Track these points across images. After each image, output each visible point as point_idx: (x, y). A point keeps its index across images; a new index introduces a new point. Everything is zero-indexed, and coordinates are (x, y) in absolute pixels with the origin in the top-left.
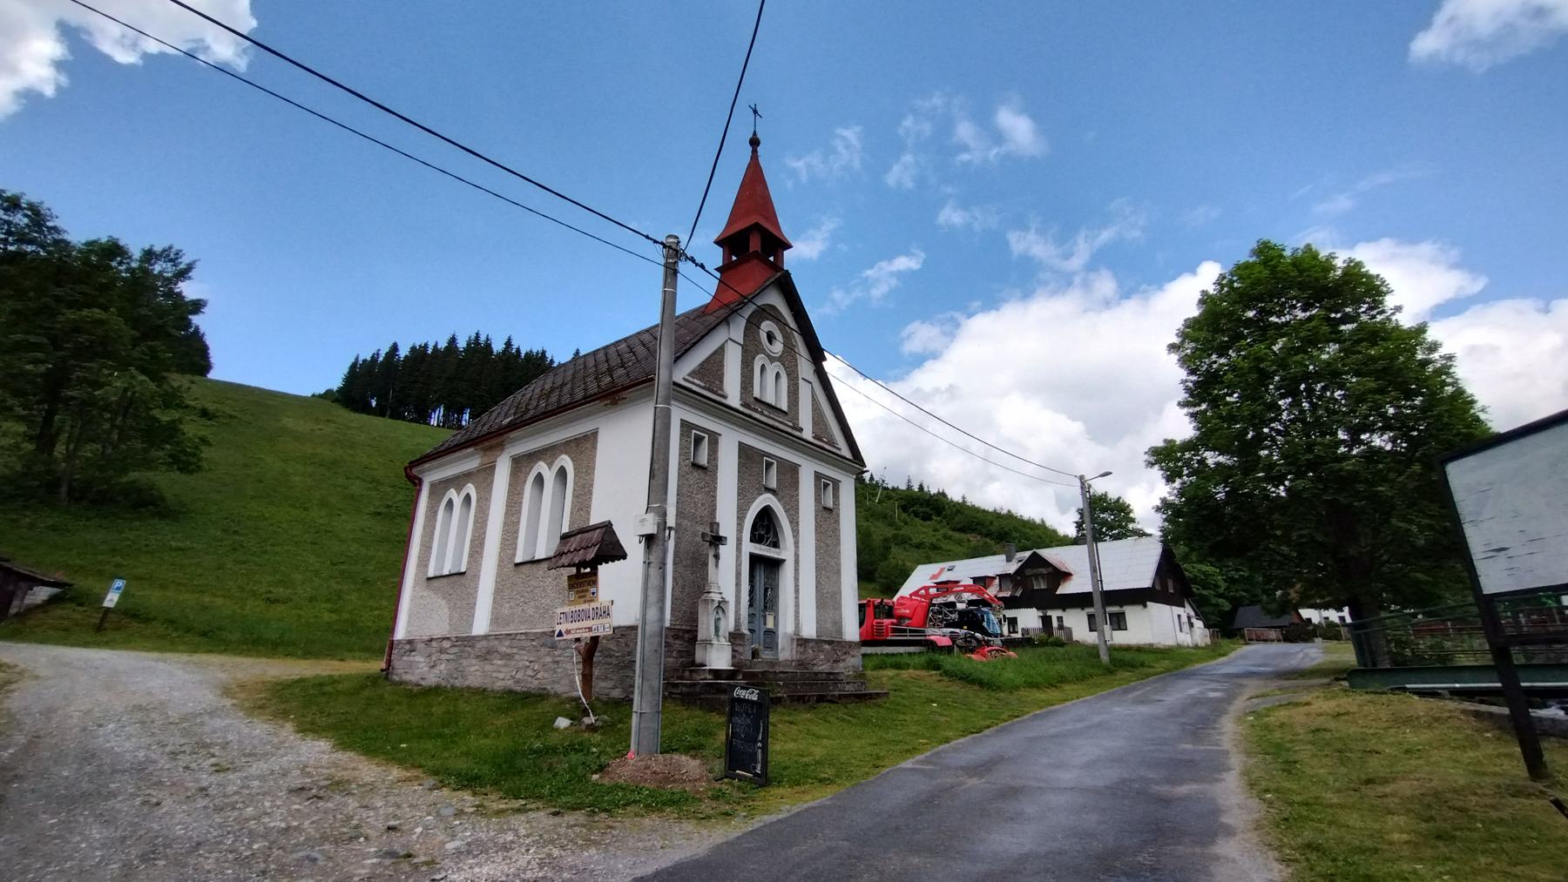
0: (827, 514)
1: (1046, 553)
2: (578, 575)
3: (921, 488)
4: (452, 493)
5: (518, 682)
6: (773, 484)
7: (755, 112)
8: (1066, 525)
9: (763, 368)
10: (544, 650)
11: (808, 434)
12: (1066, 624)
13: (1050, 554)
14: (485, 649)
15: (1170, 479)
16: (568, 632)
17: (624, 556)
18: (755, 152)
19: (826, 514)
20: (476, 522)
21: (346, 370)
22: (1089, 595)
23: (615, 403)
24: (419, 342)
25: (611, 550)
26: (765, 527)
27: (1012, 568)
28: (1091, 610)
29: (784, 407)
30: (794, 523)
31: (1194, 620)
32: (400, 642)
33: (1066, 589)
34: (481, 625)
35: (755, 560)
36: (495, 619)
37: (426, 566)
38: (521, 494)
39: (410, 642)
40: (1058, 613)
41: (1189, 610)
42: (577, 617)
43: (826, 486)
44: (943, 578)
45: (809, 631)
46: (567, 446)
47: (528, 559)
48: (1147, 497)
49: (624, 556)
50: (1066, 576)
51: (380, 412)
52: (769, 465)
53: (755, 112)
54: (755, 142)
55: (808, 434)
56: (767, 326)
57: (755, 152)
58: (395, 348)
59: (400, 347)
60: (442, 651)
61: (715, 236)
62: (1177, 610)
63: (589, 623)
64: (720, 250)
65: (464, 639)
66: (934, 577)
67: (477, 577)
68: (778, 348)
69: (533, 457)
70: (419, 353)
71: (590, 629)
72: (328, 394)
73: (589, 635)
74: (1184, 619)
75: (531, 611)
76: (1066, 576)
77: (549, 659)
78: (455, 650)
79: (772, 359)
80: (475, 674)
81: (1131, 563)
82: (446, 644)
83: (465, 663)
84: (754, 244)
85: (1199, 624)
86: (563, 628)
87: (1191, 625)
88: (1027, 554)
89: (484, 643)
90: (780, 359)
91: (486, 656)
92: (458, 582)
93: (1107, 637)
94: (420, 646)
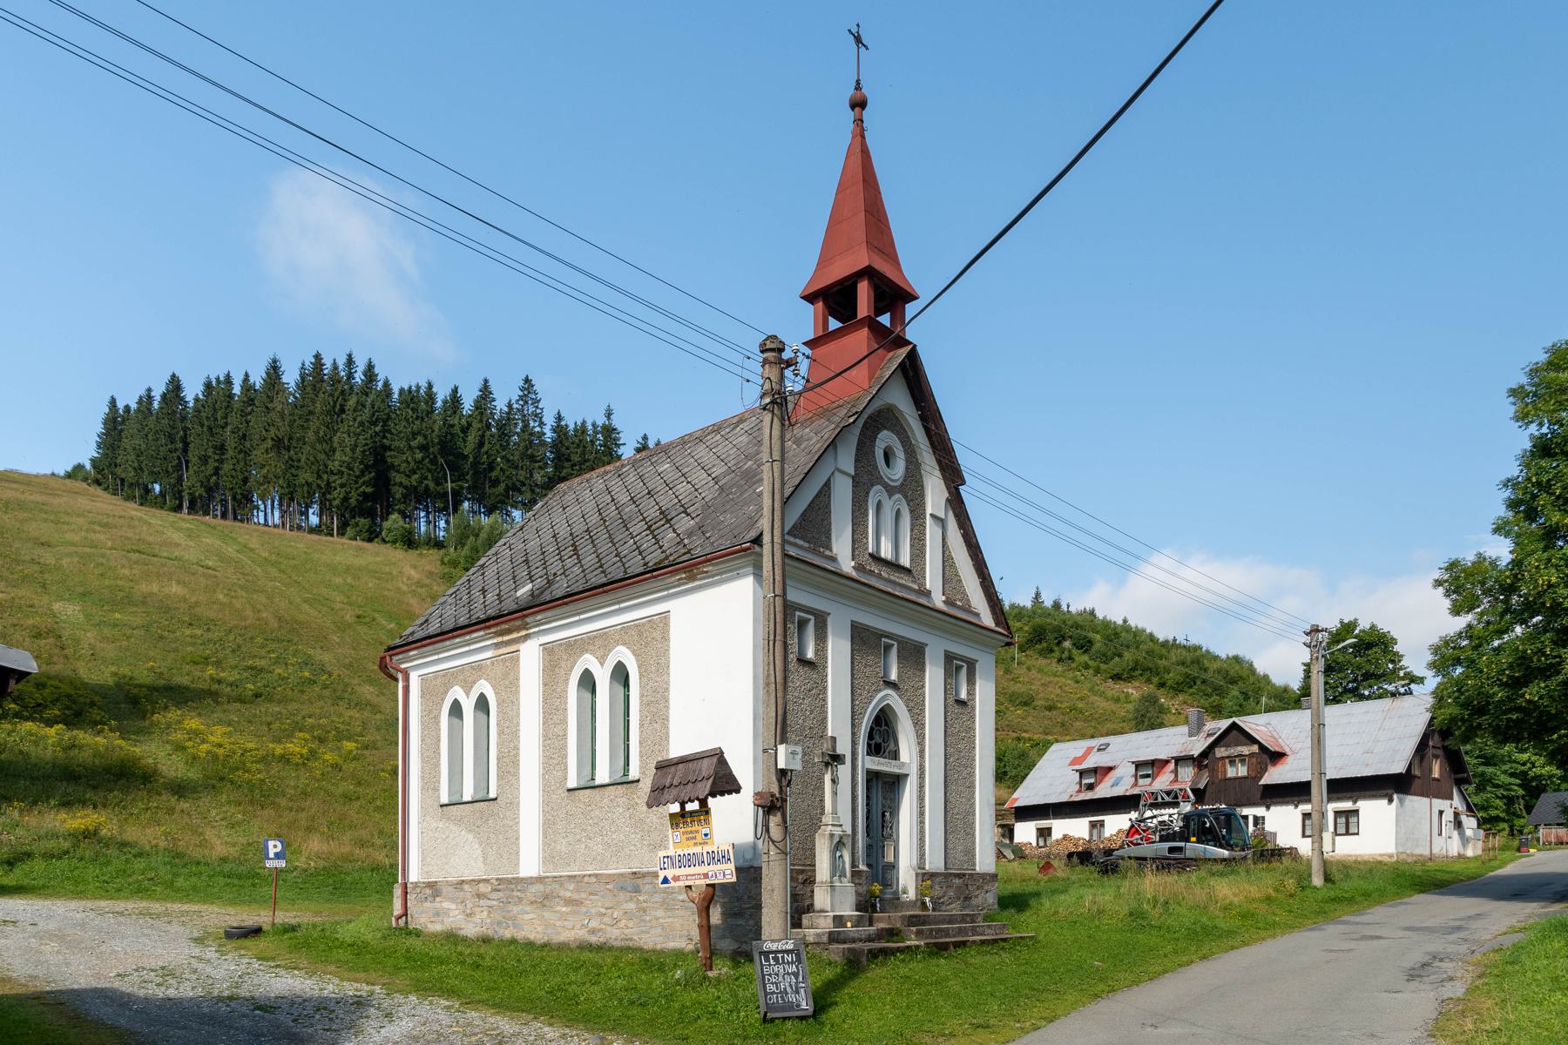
0: (959, 707)
1: (1251, 723)
2: (683, 814)
3: (1057, 605)
4: (457, 692)
5: (593, 932)
6: (893, 676)
7: (858, 40)
8: (1284, 662)
9: (879, 506)
10: (622, 896)
11: (938, 600)
12: (1269, 827)
13: (1259, 725)
14: (544, 891)
15: (1456, 611)
16: (676, 879)
17: (738, 790)
18: (859, 121)
19: (957, 709)
20: (501, 733)
21: (100, 428)
22: (1308, 784)
23: (692, 578)
24: (216, 372)
25: (725, 783)
26: (881, 736)
27: (1198, 746)
28: (1307, 808)
29: (905, 561)
30: (919, 725)
31: (1463, 818)
32: (416, 885)
33: (1276, 775)
34: (530, 864)
35: (873, 777)
36: (549, 857)
37: (436, 789)
38: (563, 697)
39: (431, 885)
40: (1260, 811)
41: (1457, 802)
42: (688, 860)
43: (959, 668)
44: (1089, 763)
45: (935, 862)
46: (625, 634)
47: (583, 783)
48: (1420, 621)
49: (738, 790)
50: (1277, 757)
51: (160, 502)
52: (888, 648)
53: (858, 40)
54: (859, 104)
55: (938, 600)
56: (885, 439)
57: (859, 121)
58: (175, 385)
59: (184, 383)
60: (479, 896)
61: (799, 290)
62: (1439, 804)
63: (704, 869)
64: (809, 311)
65: (509, 881)
66: (1076, 761)
67: (514, 805)
68: (898, 471)
69: (576, 647)
70: (217, 391)
71: (706, 876)
72: (76, 472)
73: (703, 882)
74: (1448, 816)
75: (600, 848)
76: (1277, 757)
77: (632, 906)
78: (495, 895)
79: (891, 491)
80: (532, 926)
81: (1382, 732)
82: (484, 888)
83: (515, 909)
84: (863, 298)
85: (1470, 823)
86: (669, 873)
87: (1458, 824)
88: (1224, 724)
89: (539, 887)
90: (901, 489)
91: (544, 901)
92: (486, 807)
93: (1327, 847)
94: (446, 890)
